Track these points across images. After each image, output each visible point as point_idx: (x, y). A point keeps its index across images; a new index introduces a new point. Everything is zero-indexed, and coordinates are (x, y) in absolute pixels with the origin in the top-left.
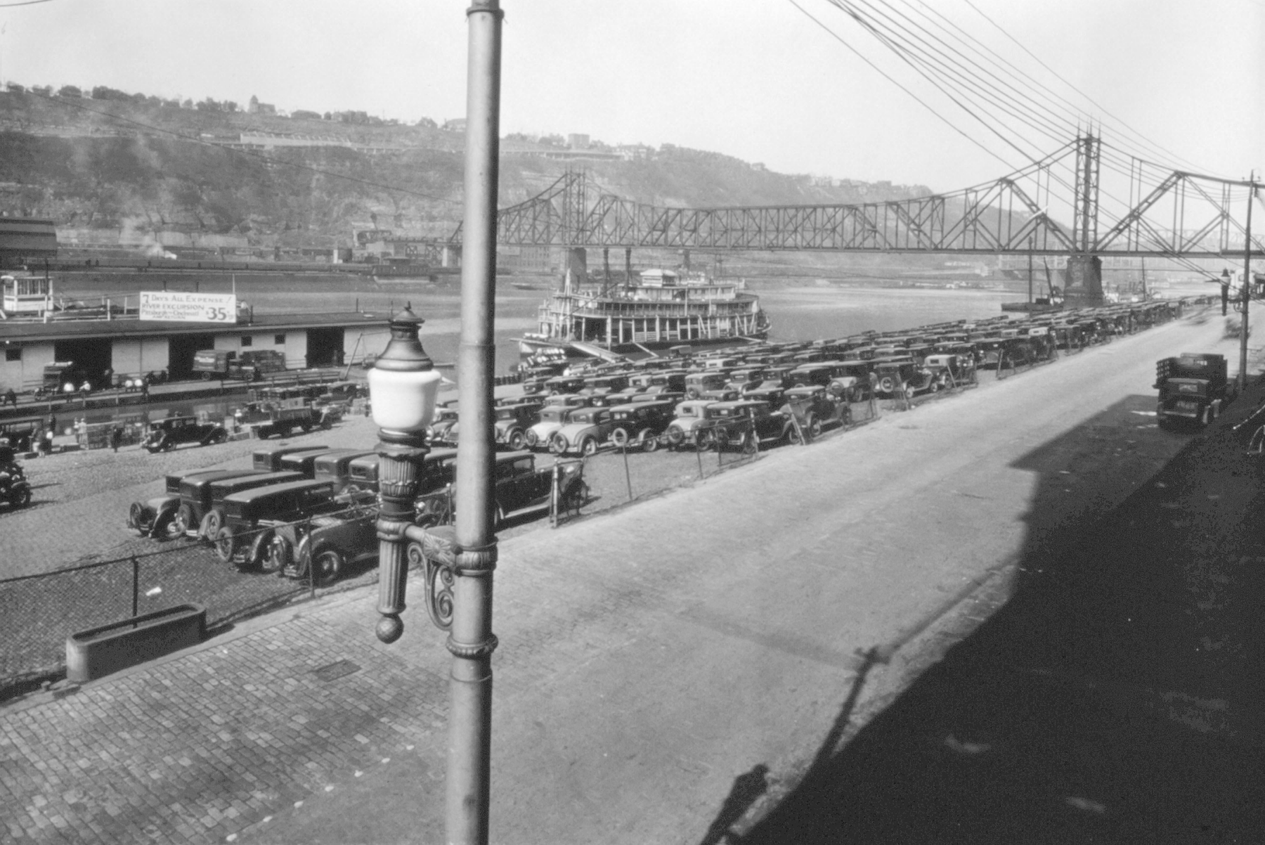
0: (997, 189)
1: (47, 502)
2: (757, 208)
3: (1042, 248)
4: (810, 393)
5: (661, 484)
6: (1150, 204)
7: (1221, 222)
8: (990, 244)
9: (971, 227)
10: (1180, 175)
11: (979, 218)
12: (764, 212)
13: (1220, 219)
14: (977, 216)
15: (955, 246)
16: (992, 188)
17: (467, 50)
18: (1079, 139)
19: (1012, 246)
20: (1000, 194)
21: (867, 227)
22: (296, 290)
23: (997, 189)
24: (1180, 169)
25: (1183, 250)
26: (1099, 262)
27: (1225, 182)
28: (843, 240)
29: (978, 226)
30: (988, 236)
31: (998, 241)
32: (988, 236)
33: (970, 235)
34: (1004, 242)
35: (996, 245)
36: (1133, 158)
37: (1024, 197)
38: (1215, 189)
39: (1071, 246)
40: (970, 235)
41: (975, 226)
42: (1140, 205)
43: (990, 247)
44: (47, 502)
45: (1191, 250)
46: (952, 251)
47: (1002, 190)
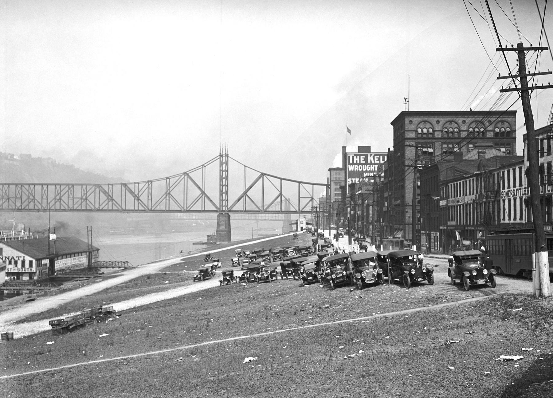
2: (26, 184)
3: (59, 208)
4: (218, 284)
5: (87, 297)
8: (91, 207)
10: (263, 174)
12: (45, 187)
13: (201, 195)
14: (170, 192)
15: (106, 208)
16: (181, 176)
19: (101, 208)
21: (110, 198)
23: (183, 176)
24: (264, 172)
25: (188, 209)
26: (229, 216)
28: (16, 206)
30: (117, 205)
31: (68, 205)
32: (117, 205)
33: (58, 203)
34: (150, 208)
35: (297, 210)
36: (244, 166)
38: (277, 182)
45: (191, 209)
46: (105, 211)
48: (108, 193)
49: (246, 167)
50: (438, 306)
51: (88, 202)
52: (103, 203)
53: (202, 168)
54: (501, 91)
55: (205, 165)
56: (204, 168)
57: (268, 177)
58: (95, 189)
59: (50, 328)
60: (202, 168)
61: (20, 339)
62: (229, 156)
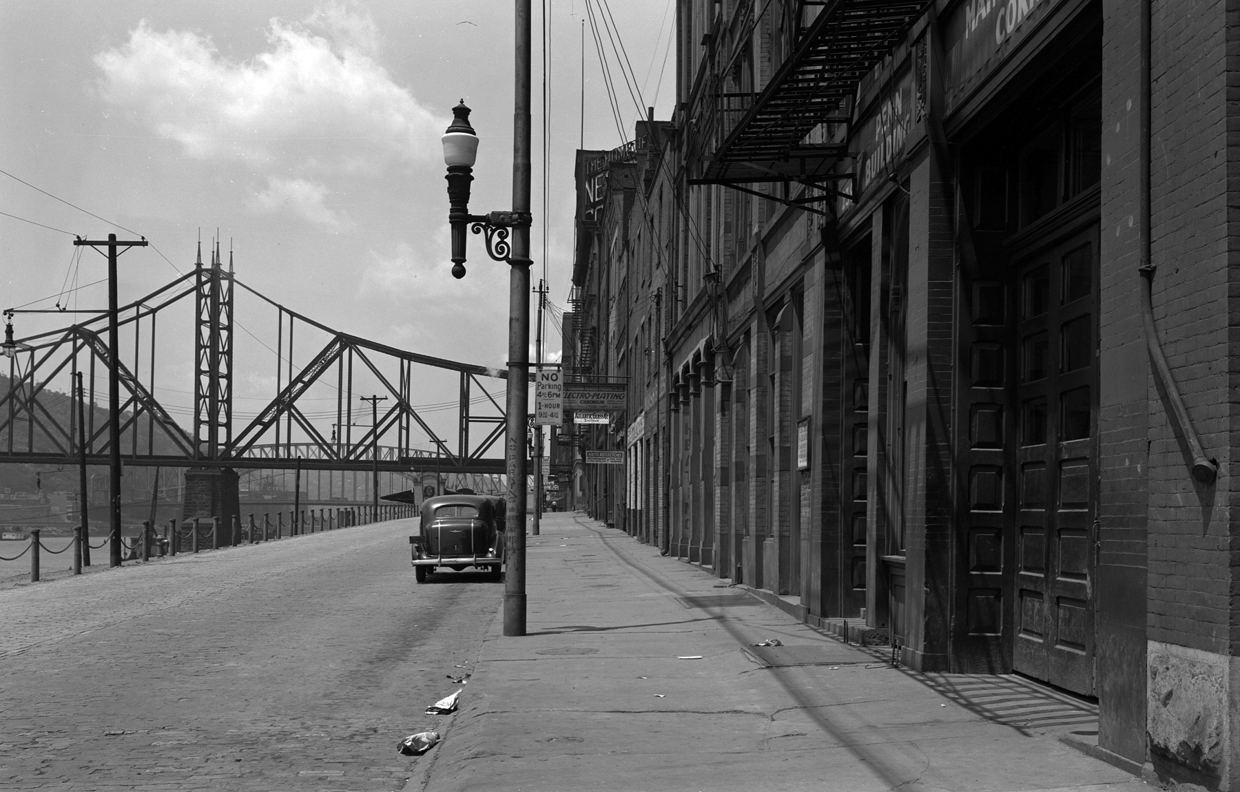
0: (67, 348)
1: (1148, 347)
6: (307, 385)
7: (399, 417)
9: (23, 414)
10: (346, 342)
11: (37, 397)
13: (397, 412)
16: (57, 345)
17: (870, 362)
18: (199, 271)
20: (73, 357)
22: (815, 395)
23: (67, 348)
27: (403, 355)
29: (38, 413)
30: (52, 429)
36: (281, 308)
37: (316, 368)
39: (191, 450)
40: (21, 428)
41: (30, 412)
42: (292, 384)
43: (54, 450)
44: (1148, 347)
47: (76, 350)
48: (135, 380)
49: (292, 314)
50: (1225, 723)
51: (285, 384)
52: (878, 207)
53: (138, 317)
54: (75, 243)
55: (153, 303)
56: (146, 322)
57: (364, 350)
58: (76, 350)
59: (777, 175)
60: (138, 317)
61: (681, 106)
62: (235, 277)
